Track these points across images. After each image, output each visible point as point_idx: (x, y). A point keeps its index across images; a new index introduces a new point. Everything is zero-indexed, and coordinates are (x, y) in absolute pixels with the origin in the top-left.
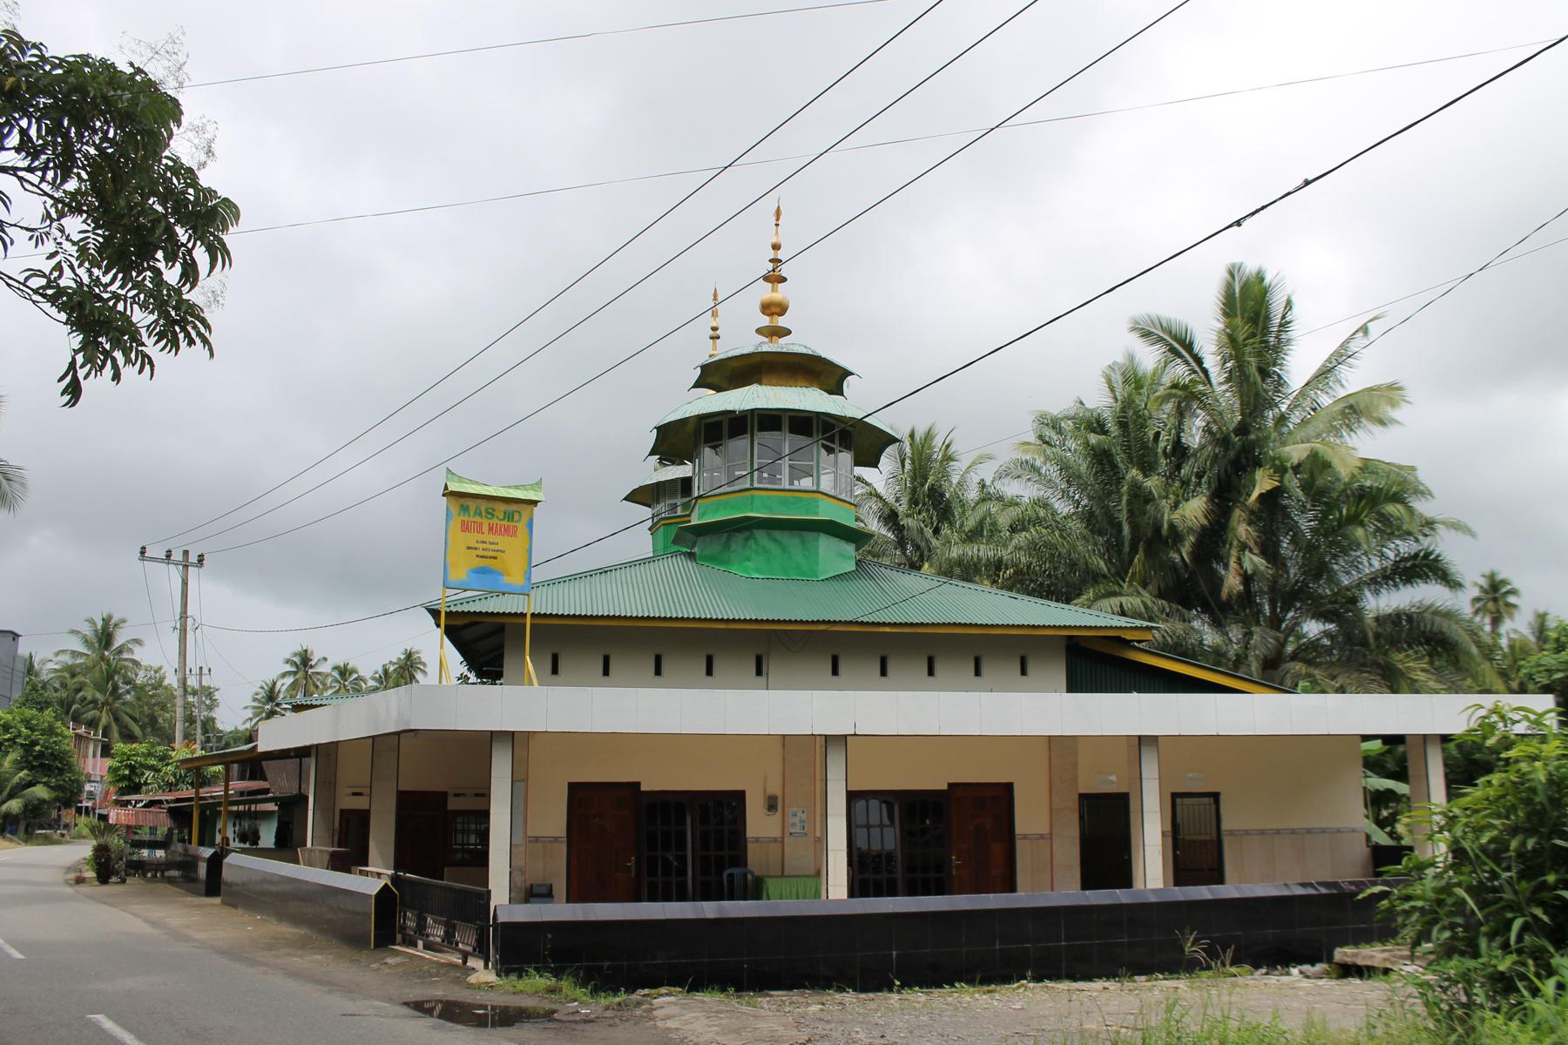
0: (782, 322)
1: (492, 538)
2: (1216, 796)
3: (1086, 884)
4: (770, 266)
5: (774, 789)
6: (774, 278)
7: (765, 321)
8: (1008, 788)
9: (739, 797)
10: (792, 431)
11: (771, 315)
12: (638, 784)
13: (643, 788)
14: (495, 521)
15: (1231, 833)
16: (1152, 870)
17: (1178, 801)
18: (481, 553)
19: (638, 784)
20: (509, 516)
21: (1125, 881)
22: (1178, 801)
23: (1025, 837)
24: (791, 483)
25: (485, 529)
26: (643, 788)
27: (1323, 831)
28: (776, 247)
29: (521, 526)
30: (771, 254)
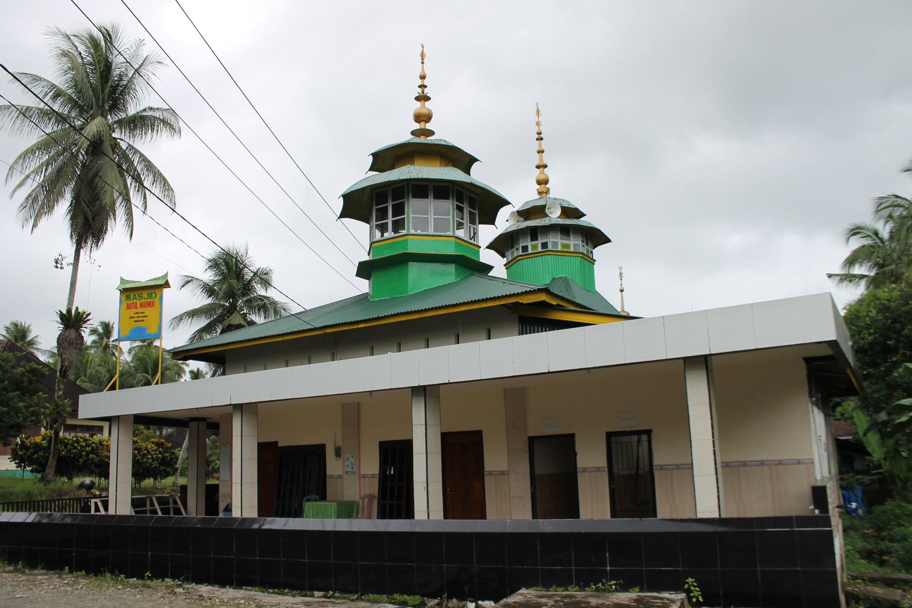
0: (429, 126)
1: (142, 310)
2: (609, 435)
3: (382, 515)
4: (420, 90)
5: (339, 443)
6: (423, 98)
7: (417, 126)
8: (479, 433)
9: (322, 447)
10: (436, 197)
11: (419, 122)
12: (276, 443)
13: (280, 445)
14: (143, 300)
15: (662, 467)
16: (428, 505)
17: (613, 439)
18: (136, 319)
19: (276, 443)
20: (150, 296)
21: (409, 513)
22: (613, 439)
23: (490, 473)
24: (382, 236)
25: (138, 306)
26: (280, 445)
27: (762, 463)
28: (423, 77)
29: (157, 301)
30: (420, 82)
